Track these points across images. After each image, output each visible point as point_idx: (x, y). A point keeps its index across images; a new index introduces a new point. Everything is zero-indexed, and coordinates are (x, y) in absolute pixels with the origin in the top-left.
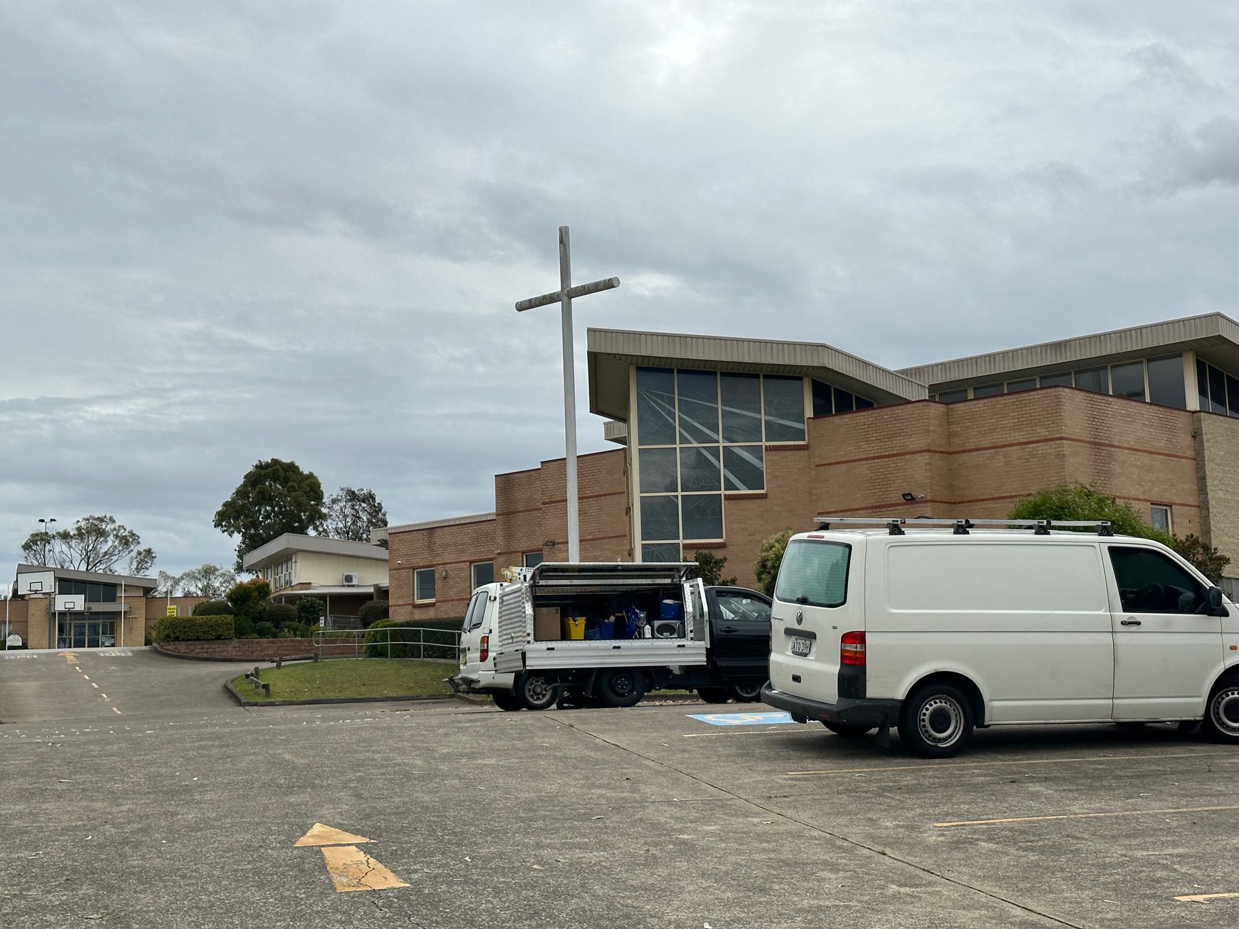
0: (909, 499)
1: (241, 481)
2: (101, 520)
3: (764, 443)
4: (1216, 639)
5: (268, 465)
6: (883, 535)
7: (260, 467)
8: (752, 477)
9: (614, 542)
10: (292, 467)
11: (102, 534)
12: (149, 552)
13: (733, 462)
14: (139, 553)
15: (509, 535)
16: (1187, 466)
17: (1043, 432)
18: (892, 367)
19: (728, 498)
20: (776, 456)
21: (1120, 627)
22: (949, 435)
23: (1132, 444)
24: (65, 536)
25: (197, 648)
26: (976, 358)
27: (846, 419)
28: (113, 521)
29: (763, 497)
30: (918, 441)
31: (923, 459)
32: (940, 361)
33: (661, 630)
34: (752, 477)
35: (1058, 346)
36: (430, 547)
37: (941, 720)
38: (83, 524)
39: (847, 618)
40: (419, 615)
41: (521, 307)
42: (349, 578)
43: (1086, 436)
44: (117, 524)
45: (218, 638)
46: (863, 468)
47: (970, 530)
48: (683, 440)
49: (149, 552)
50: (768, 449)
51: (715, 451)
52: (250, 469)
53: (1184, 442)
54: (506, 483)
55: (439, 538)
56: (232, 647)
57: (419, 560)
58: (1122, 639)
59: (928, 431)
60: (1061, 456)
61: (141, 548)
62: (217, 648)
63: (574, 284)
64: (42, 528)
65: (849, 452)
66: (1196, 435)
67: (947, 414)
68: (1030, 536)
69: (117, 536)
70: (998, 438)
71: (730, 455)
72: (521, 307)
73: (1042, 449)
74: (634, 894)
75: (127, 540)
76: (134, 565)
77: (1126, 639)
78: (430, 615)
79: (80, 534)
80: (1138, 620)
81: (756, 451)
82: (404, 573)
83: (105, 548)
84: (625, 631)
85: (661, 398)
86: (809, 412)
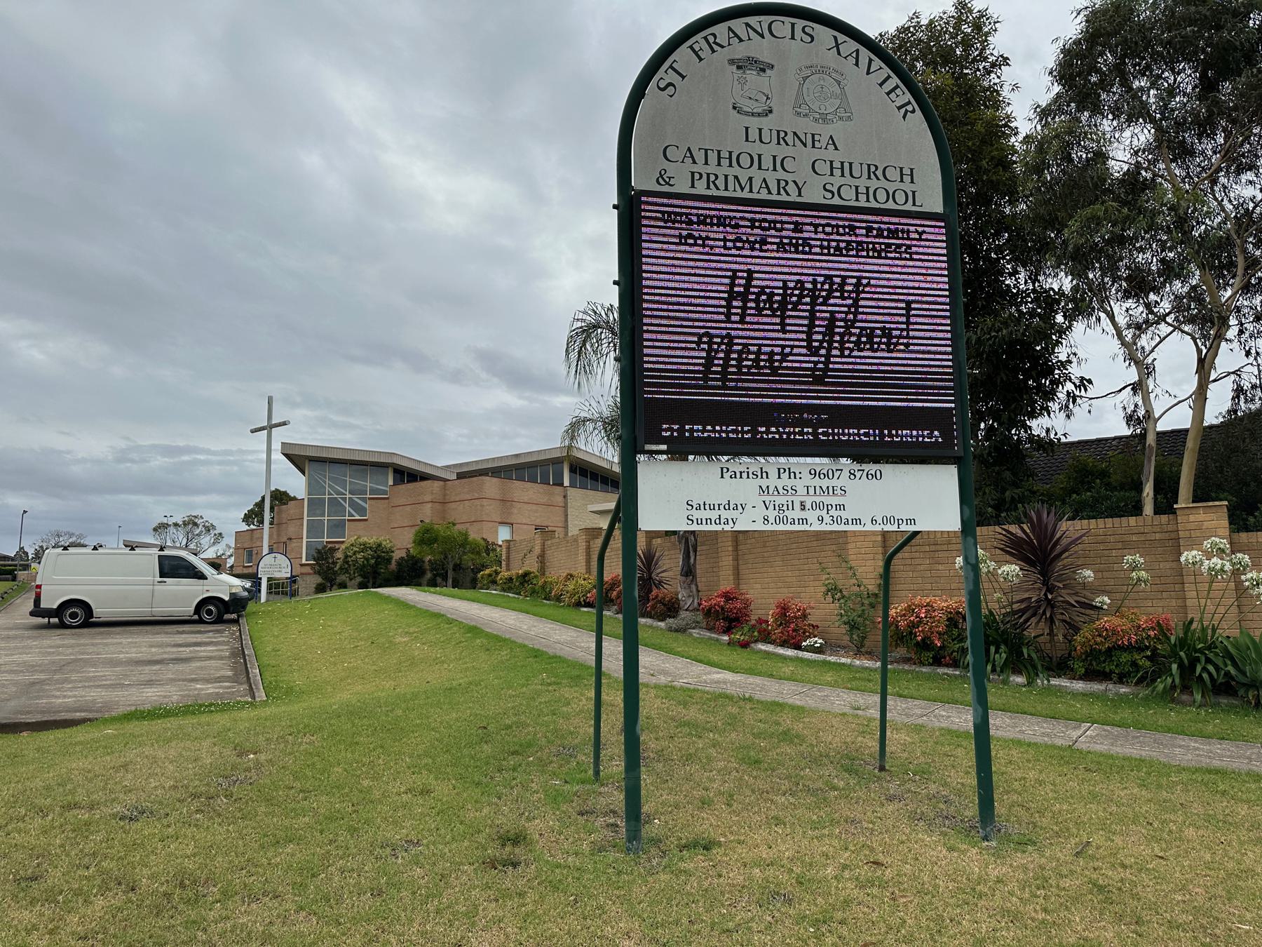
2: (196, 517)
3: (368, 496)
4: (201, 588)
8: (362, 511)
11: (195, 524)
12: (220, 534)
13: (353, 504)
14: (215, 535)
16: (560, 511)
17: (476, 495)
18: (439, 465)
19: (349, 520)
20: (373, 502)
21: (156, 583)
22: (445, 495)
23: (526, 501)
24: (176, 525)
28: (202, 517)
29: (366, 520)
30: (428, 498)
31: (429, 505)
34: (362, 511)
35: (517, 456)
38: (186, 519)
41: (252, 432)
43: (498, 497)
44: (205, 519)
46: (408, 508)
49: (220, 534)
50: (370, 499)
51: (344, 499)
52: (282, 489)
53: (560, 499)
57: (246, 545)
59: (432, 493)
60: (482, 506)
61: (216, 532)
63: (274, 422)
64: (165, 520)
67: (445, 485)
69: (204, 526)
71: (351, 501)
72: (252, 432)
73: (477, 502)
76: (212, 541)
77: (159, 588)
79: (185, 524)
82: (240, 551)
83: (197, 532)
85: (320, 474)
86: (391, 482)
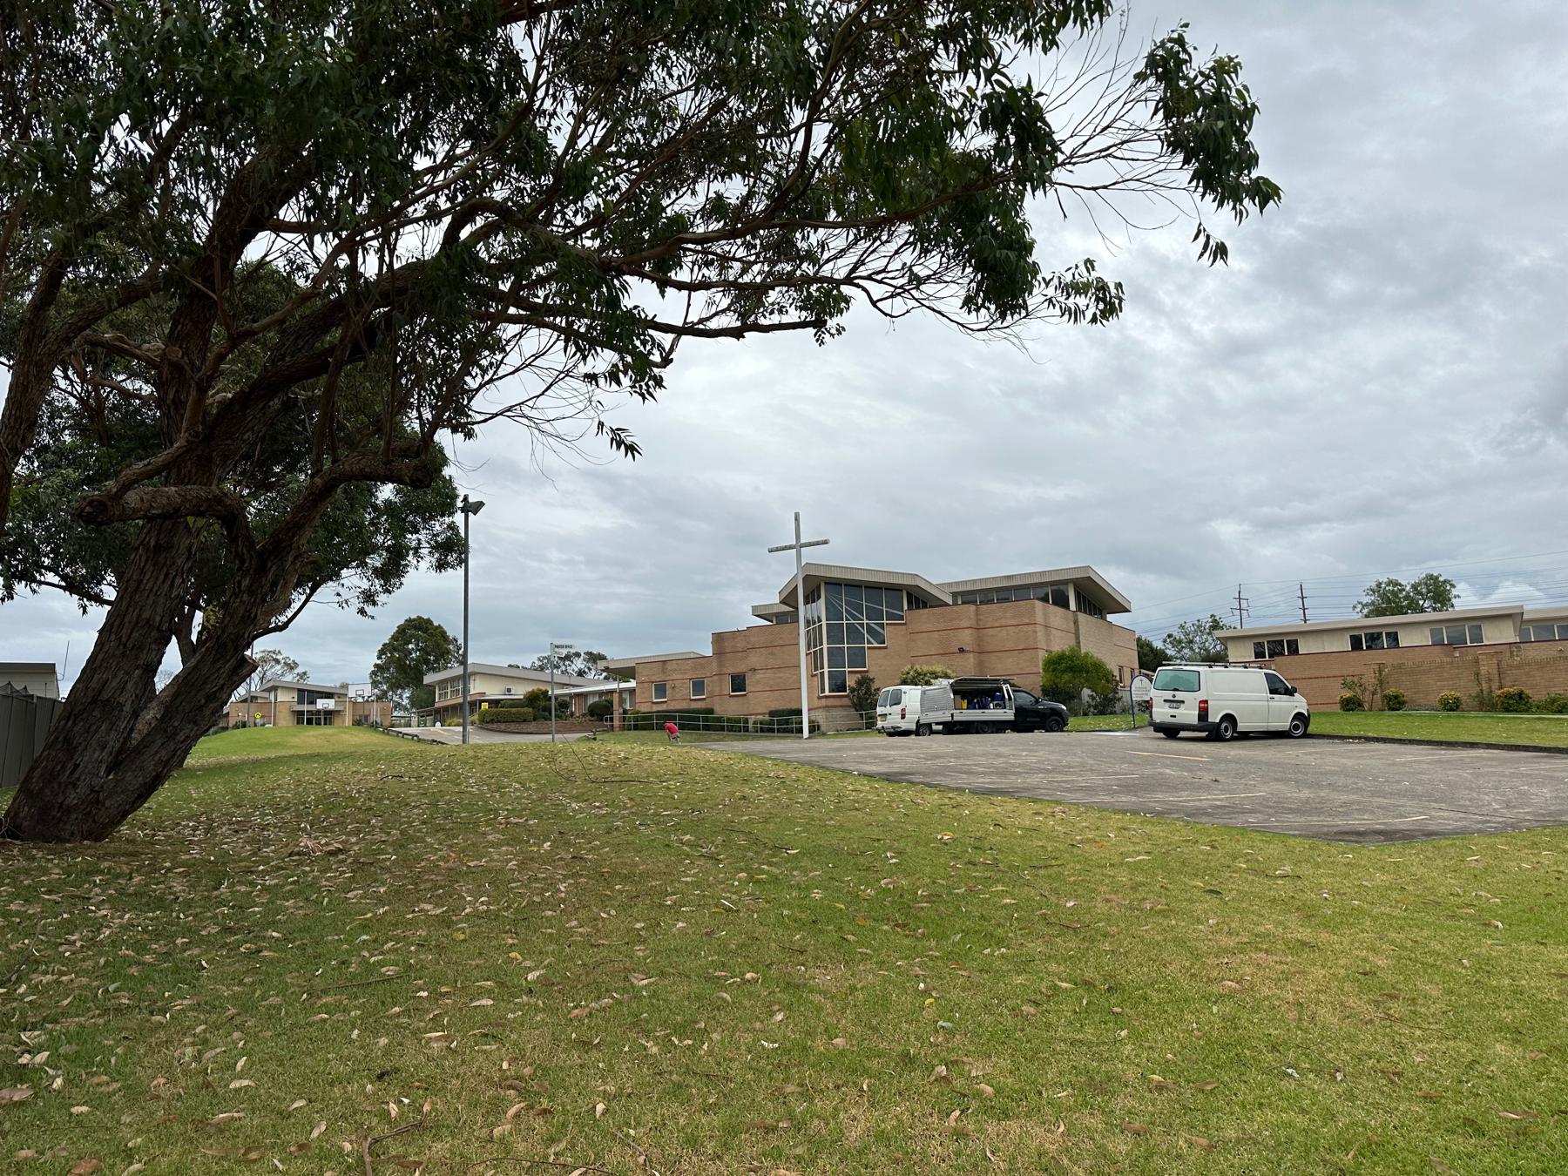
0: (961, 650)
1: (395, 629)
5: (414, 620)
6: (1207, 668)
7: (409, 621)
9: (792, 669)
10: (429, 621)
15: (721, 665)
22: (978, 620)
25: (512, 727)
26: (966, 582)
27: (926, 611)
29: (886, 648)
31: (967, 631)
32: (946, 581)
33: (997, 705)
36: (664, 671)
37: (1226, 729)
39: (1201, 696)
40: (655, 708)
42: (509, 690)
45: (525, 721)
46: (936, 635)
47: (538, 663)
48: (847, 619)
54: (719, 638)
55: (669, 666)
56: (532, 726)
58: (1271, 703)
62: (523, 727)
63: (803, 541)
65: (929, 627)
66: (1076, 622)
68: (1222, 668)
70: (1004, 622)
74: (336, 938)
75: (291, 666)
78: (664, 707)
80: (1167, 704)
81: (882, 626)
82: (646, 685)
84: (984, 707)
86: (906, 607)
